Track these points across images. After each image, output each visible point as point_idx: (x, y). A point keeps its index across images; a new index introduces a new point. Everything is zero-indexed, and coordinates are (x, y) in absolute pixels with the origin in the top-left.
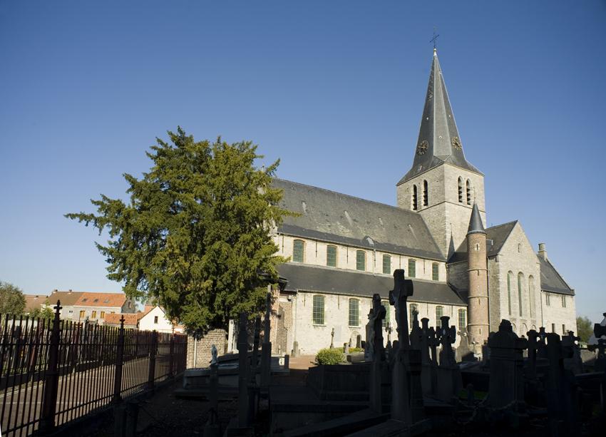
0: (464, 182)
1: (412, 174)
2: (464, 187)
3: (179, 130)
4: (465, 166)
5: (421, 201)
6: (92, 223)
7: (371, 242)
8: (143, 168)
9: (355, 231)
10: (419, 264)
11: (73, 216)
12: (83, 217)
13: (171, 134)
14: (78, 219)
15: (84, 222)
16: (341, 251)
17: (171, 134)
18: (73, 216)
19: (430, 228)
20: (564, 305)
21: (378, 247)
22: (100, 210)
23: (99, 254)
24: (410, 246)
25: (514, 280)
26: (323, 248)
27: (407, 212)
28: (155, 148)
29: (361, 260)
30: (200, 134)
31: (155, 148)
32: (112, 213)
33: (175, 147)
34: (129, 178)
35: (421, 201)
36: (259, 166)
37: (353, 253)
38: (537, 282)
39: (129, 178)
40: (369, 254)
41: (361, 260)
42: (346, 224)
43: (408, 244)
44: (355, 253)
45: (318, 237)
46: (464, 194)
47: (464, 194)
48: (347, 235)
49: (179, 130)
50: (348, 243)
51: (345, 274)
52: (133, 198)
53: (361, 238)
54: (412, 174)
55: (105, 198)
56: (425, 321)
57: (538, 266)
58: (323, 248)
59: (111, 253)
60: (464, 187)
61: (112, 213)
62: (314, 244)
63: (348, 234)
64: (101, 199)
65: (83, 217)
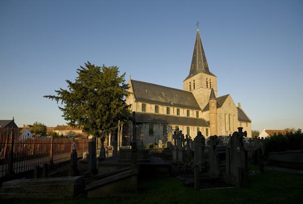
0: (208, 79)
1: (189, 77)
2: (209, 81)
3: (88, 62)
4: (210, 73)
5: (192, 88)
6: (54, 99)
7: (172, 104)
8: (74, 78)
9: (166, 99)
10: (191, 112)
11: (47, 97)
12: (51, 97)
13: (86, 64)
14: (48, 98)
15: (51, 99)
16: (160, 107)
17: (86, 64)
18: (47, 97)
19: (196, 98)
20: (247, 126)
21: (175, 105)
22: (59, 94)
23: (60, 111)
24: (187, 105)
25: (227, 117)
26: (153, 106)
27: (187, 92)
28: (79, 70)
29: (168, 110)
30: (97, 63)
31: (79, 70)
32: (65, 95)
33: (87, 69)
34: (68, 81)
35: (192, 88)
36: (119, 75)
37: (165, 108)
38: (236, 117)
39: (68, 81)
40: (171, 109)
41: (168, 110)
42: (163, 97)
43: (187, 104)
44: (166, 108)
45: (151, 102)
46: (209, 84)
47: (209, 84)
48: (163, 101)
49: (88, 62)
50: (163, 104)
51: (192, 119)
52: (70, 89)
53: (168, 102)
54: (189, 77)
55: (61, 89)
56: (103, 152)
57: (237, 112)
58: (153, 106)
59: (65, 110)
60: (209, 81)
61: (65, 95)
62: (192, 110)
63: (163, 101)
64: (59, 90)
65: (51, 97)
